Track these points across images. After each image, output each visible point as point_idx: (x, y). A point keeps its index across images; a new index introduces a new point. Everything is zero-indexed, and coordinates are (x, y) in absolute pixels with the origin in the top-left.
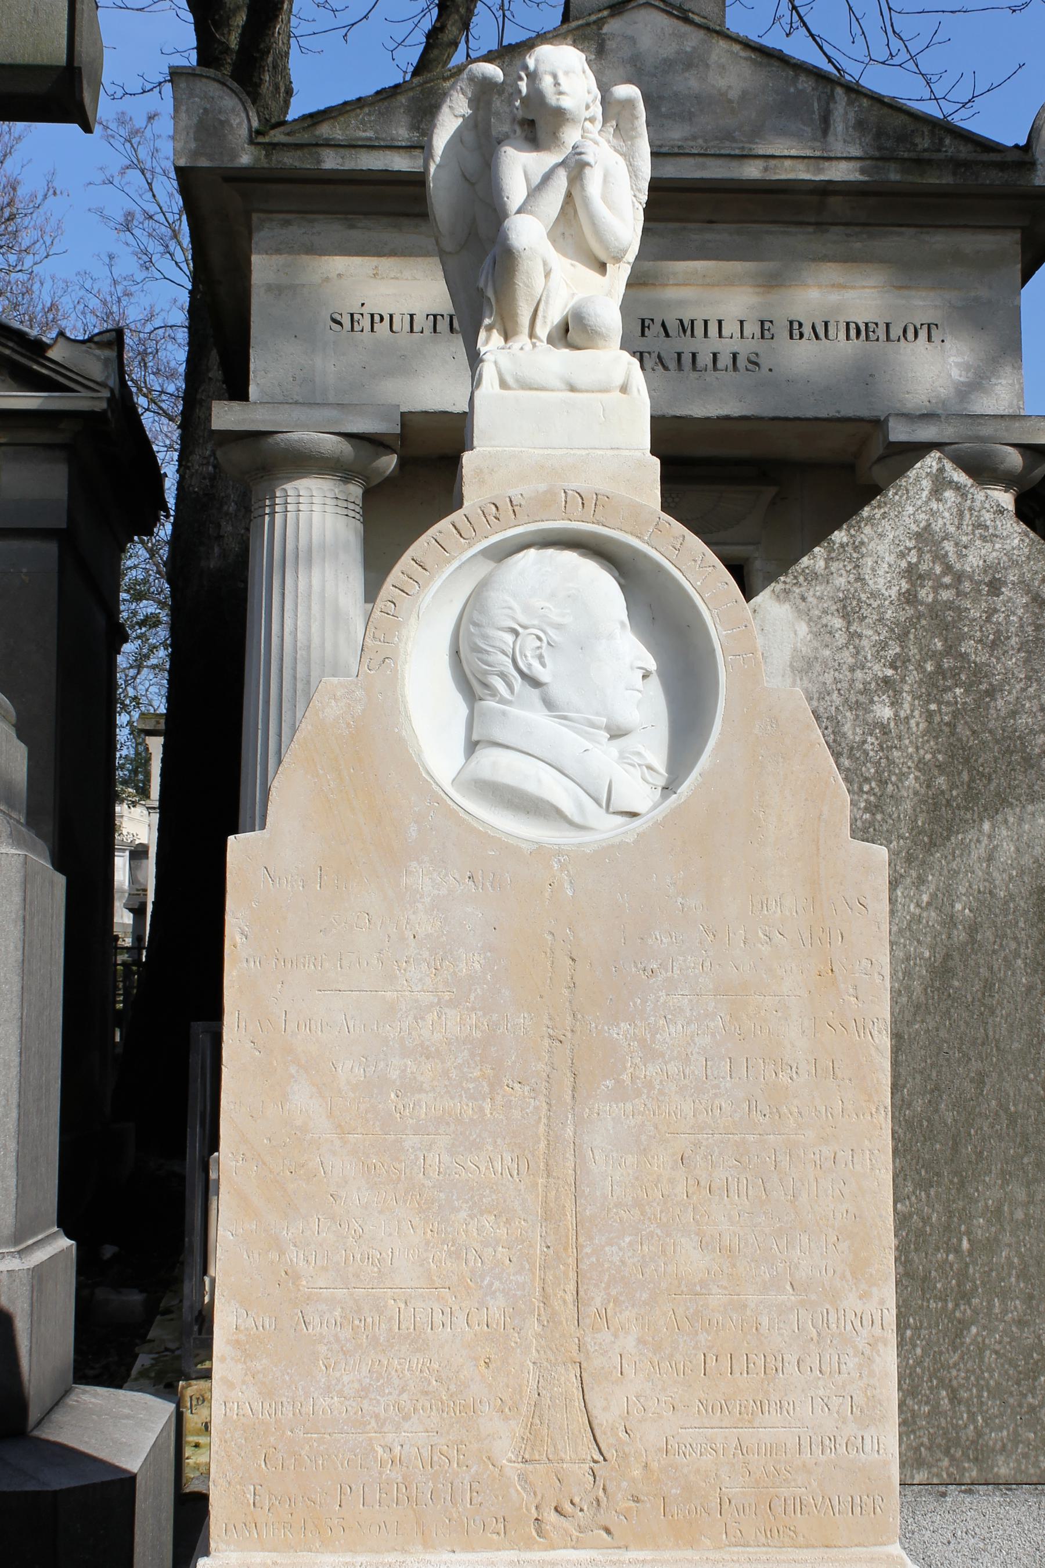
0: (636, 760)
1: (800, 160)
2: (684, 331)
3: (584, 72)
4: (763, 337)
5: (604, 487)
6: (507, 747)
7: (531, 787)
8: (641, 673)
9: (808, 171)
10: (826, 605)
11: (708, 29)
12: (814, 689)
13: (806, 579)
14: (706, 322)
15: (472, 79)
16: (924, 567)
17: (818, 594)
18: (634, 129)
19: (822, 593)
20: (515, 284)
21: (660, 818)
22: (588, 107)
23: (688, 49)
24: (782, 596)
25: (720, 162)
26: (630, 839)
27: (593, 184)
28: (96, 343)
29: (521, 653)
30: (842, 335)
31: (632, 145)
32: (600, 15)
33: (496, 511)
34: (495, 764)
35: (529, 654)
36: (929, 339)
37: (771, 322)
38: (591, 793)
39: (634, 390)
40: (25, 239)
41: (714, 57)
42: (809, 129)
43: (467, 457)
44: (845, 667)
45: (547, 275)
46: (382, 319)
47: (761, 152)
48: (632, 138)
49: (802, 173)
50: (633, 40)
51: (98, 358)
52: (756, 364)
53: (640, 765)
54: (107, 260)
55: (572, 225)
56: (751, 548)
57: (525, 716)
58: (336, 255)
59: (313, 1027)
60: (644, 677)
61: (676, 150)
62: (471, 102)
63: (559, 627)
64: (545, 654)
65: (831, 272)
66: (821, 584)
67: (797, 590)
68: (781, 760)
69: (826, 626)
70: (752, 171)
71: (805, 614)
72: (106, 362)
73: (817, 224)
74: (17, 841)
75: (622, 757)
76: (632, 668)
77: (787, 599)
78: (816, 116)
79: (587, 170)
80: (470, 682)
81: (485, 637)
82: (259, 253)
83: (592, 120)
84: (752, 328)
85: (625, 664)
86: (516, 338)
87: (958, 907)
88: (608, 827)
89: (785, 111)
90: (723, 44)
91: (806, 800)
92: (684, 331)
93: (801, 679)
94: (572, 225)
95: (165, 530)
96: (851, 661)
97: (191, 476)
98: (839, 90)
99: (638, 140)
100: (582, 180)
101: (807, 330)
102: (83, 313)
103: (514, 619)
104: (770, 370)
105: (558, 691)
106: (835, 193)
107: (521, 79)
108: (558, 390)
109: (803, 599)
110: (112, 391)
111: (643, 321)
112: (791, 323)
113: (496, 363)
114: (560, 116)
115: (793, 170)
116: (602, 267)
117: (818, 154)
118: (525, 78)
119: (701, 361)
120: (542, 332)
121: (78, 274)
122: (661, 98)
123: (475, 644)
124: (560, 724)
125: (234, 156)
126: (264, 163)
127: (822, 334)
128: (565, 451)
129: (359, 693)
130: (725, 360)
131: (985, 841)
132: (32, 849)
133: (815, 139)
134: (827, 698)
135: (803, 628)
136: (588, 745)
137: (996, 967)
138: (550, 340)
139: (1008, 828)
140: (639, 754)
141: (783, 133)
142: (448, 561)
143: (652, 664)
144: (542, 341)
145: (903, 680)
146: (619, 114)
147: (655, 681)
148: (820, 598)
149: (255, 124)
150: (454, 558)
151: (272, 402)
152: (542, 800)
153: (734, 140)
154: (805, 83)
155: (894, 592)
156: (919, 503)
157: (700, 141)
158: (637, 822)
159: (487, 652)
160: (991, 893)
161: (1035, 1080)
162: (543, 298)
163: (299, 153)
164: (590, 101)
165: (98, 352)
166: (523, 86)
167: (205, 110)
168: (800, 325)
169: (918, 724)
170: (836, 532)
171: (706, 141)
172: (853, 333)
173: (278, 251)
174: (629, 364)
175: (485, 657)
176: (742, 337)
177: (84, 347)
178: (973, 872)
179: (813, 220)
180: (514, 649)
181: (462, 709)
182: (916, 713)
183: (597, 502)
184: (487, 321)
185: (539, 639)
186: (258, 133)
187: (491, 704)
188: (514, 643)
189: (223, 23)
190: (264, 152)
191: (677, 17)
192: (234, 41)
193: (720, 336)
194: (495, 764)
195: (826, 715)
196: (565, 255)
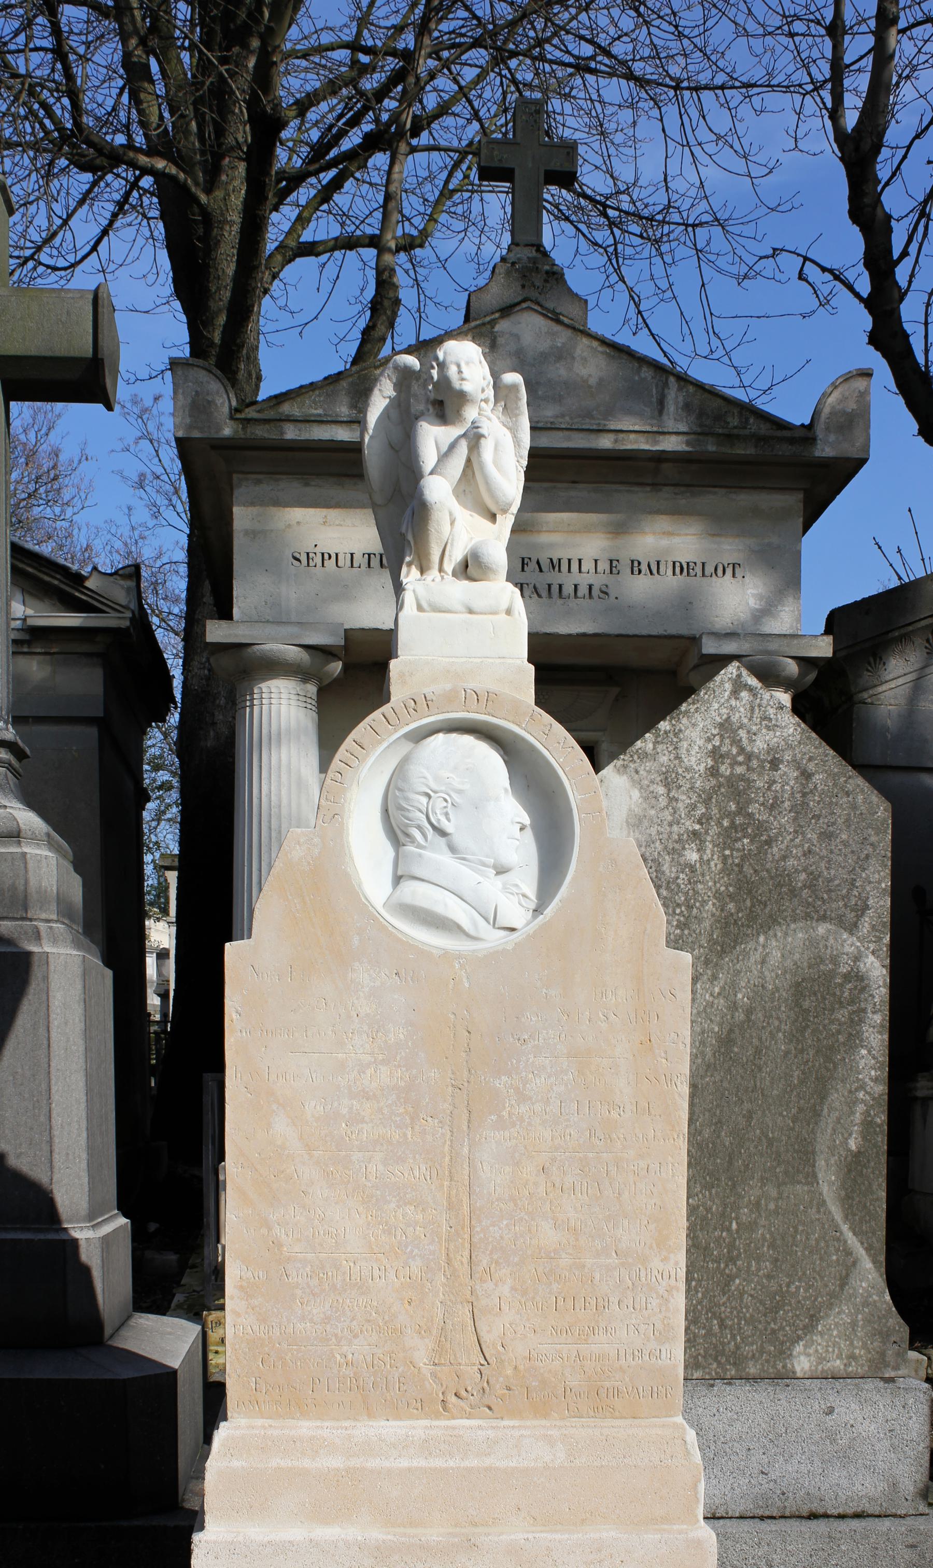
0: (515, 890)
2: (554, 568)
3: (480, 362)
4: (611, 573)
5: (493, 687)
6: (423, 880)
7: (439, 909)
8: (519, 826)
9: (647, 443)
14: (569, 560)
15: (396, 367)
16: (724, 749)
18: (518, 408)
20: (428, 530)
21: (531, 932)
22: (483, 391)
23: (559, 345)
24: (622, 769)
25: (581, 435)
26: (510, 947)
28: (120, 575)
30: (670, 571)
31: (516, 421)
32: (493, 317)
33: (414, 705)
35: (438, 812)
36: (734, 576)
40: (66, 495)
41: (578, 352)
43: (393, 663)
44: (665, 823)
45: (452, 523)
46: (330, 557)
47: (612, 428)
48: (517, 416)
49: (643, 445)
51: (122, 587)
52: (606, 593)
55: (471, 482)
56: (600, 734)
59: (288, 1078)
60: (521, 829)
61: (549, 425)
62: (395, 385)
63: (460, 792)
64: (450, 812)
65: (663, 523)
70: (605, 442)
71: (637, 783)
72: (128, 590)
73: (653, 485)
74: (77, 945)
75: (505, 888)
76: (512, 823)
77: (625, 772)
78: (654, 400)
79: (483, 441)
80: (396, 833)
81: (407, 799)
82: (239, 505)
83: (486, 401)
84: (603, 566)
85: (507, 820)
87: (740, 996)
88: (494, 938)
90: (585, 341)
92: (554, 568)
94: (471, 482)
95: (174, 718)
96: (670, 818)
98: (672, 379)
101: (644, 567)
103: (428, 786)
105: (459, 839)
106: (667, 460)
107: (433, 368)
110: (133, 612)
111: (523, 559)
112: (632, 562)
113: (414, 591)
114: (462, 398)
115: (636, 442)
116: (493, 517)
117: (655, 429)
120: (449, 567)
121: (106, 522)
122: (538, 383)
125: (219, 429)
128: (465, 659)
129: (316, 840)
130: (583, 590)
131: (760, 949)
132: (88, 950)
133: (653, 418)
134: (652, 845)
135: (636, 794)
136: (481, 879)
137: (764, 1038)
139: (777, 940)
140: (517, 886)
141: (629, 412)
143: (527, 820)
145: (707, 833)
146: (506, 396)
147: (529, 833)
148: (649, 772)
151: (248, 622)
152: (447, 919)
154: (647, 373)
155: (702, 768)
156: (722, 701)
157: (567, 418)
158: (515, 935)
159: (408, 810)
160: (763, 986)
161: (787, 1116)
163: (267, 426)
165: (122, 582)
168: (639, 563)
169: (716, 865)
171: (571, 418)
172: (678, 570)
173: (253, 504)
174: (512, 592)
175: (406, 814)
177: (111, 579)
178: (751, 972)
180: (427, 808)
182: (715, 857)
183: (488, 699)
184: (408, 559)
185: (446, 800)
186: (237, 410)
187: (410, 848)
188: (428, 803)
189: (209, 323)
191: (551, 319)
192: (217, 337)
193: (580, 571)
196: (466, 507)
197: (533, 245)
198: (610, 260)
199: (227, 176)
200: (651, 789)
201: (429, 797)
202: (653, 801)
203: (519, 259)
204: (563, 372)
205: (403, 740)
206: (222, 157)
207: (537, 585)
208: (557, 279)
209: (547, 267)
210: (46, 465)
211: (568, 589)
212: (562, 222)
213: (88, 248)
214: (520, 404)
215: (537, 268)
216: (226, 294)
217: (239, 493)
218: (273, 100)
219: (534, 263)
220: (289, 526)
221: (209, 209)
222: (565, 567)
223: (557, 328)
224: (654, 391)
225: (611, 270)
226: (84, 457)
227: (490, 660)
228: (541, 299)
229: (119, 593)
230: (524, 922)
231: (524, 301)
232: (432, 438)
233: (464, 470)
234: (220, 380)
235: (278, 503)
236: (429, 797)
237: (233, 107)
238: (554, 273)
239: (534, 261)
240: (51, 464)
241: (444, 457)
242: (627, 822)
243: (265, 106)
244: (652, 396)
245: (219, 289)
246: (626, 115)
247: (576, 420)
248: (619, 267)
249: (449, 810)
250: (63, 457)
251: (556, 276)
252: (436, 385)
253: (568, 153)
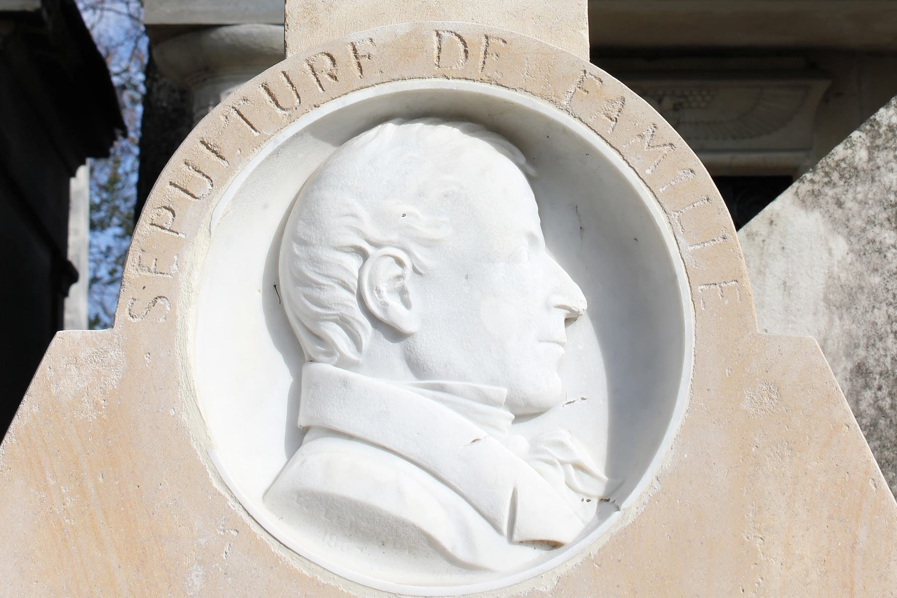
0: (557, 454)
5: (499, 26)
7: (386, 503)
8: (562, 315)
10: (871, 212)
12: (860, 332)
13: (842, 177)
17: (860, 197)
19: (866, 196)
21: (594, 551)
24: (809, 200)
26: (546, 586)
33: (331, 68)
34: (334, 467)
35: (383, 287)
38: (486, 513)
53: (563, 463)
56: (801, 155)
57: (375, 386)
60: (568, 321)
63: (430, 244)
64: (410, 287)
66: (864, 182)
67: (830, 192)
68: (787, 453)
69: (874, 242)
71: (843, 226)
75: (535, 449)
76: (548, 307)
77: (816, 205)
80: (296, 336)
81: (315, 262)
85: (534, 301)
91: (831, 518)
93: (841, 318)
97: (159, 89)
103: (359, 232)
105: (432, 345)
123: (301, 272)
124: (434, 398)
129: (114, 354)
134: (879, 345)
135: (840, 245)
136: (479, 431)
140: (561, 445)
143: (579, 301)
147: (585, 329)
148: (864, 203)
150: (267, 139)
152: (405, 524)
158: (558, 558)
159: (319, 285)
170: (882, 111)
175: (316, 293)
181: (279, 374)
183: (491, 49)
185: (400, 263)
188: (361, 270)
194: (334, 467)
195: (879, 369)
200: (870, 235)
201: (363, 254)
205: (310, 139)
230: (578, 526)
236: (363, 254)
242: (826, 299)
249: (409, 282)
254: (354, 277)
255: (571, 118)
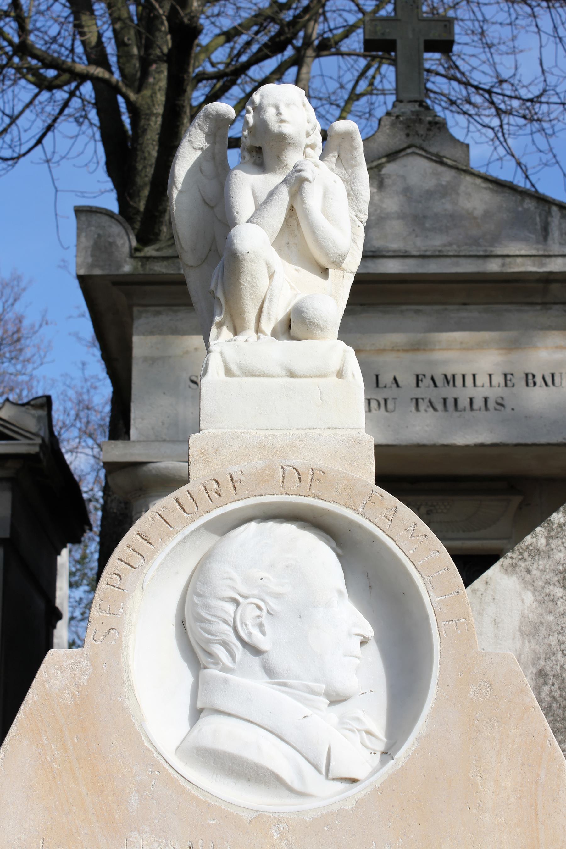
0: (355, 725)
1: (528, 258)
2: (448, 382)
3: (304, 105)
4: (506, 385)
5: (320, 463)
6: (229, 715)
7: (250, 755)
8: (358, 640)
9: (534, 265)
10: (548, 577)
11: (457, 169)
13: (530, 555)
14: (464, 376)
15: (208, 116)
17: (541, 567)
18: (353, 158)
19: (545, 567)
20: (241, 284)
21: (378, 785)
22: (308, 135)
23: (444, 183)
24: (510, 569)
25: (469, 261)
26: (349, 806)
27: (313, 198)
28: (33, 406)
29: (242, 622)
31: (353, 172)
32: (380, 162)
33: (217, 488)
35: (249, 623)
37: (512, 374)
38: (312, 761)
39: (349, 374)
40: (28, 353)
41: (462, 188)
42: (533, 236)
43: (194, 438)
45: (271, 277)
47: (499, 253)
48: (353, 166)
49: (531, 267)
50: (404, 178)
51: (33, 416)
52: (502, 405)
54: (80, 366)
55: (294, 231)
56: (505, 541)
57: (244, 683)
58: (193, 334)
60: (362, 643)
61: (437, 253)
62: (208, 136)
63: (277, 596)
65: (555, 338)
66: (543, 558)
67: (522, 564)
68: (496, 724)
69: (549, 595)
70: (493, 266)
71: (531, 585)
72: (39, 419)
73: (543, 304)
75: (342, 722)
76: (350, 635)
77: (514, 572)
78: (538, 227)
79: (306, 185)
80: (195, 653)
81: (207, 607)
82: (138, 335)
83: (312, 146)
84: (498, 379)
85: (342, 629)
86: (244, 333)
88: (326, 794)
89: (518, 224)
90: (469, 179)
91: (523, 764)
92: (448, 382)
93: (529, 642)
94: (294, 231)
97: (112, 501)
98: (554, 209)
99: (358, 168)
100: (301, 194)
101: (539, 380)
102: (64, 401)
103: (234, 589)
104: (513, 409)
105: (277, 658)
106: (555, 281)
107: (248, 112)
108: (279, 376)
109: (529, 572)
110: (43, 439)
111: (417, 376)
112: (527, 375)
113: (221, 353)
114: (282, 141)
115: (523, 265)
116: (324, 272)
117: (541, 253)
118: (252, 111)
119: (461, 404)
120: (267, 326)
121: (62, 375)
122: (425, 217)
123: (198, 614)
124: (280, 691)
125: (120, 266)
126: (140, 271)
127: (549, 381)
128: (284, 432)
130: (479, 403)
133: (538, 242)
134: (553, 658)
135: (529, 597)
136: (308, 711)
138: (275, 334)
140: (358, 719)
141: (515, 238)
142: (172, 535)
143: (369, 631)
144: (266, 335)
146: (340, 145)
147: (373, 648)
148: (543, 571)
149: (134, 243)
151: (147, 441)
152: (262, 768)
153: (479, 245)
154: (529, 204)
157: (455, 247)
158: (356, 789)
159: (210, 622)
162: (268, 297)
163: (165, 263)
164: (309, 129)
165: (33, 412)
166: (250, 118)
167: (99, 236)
168: (534, 376)
170: (554, 514)
171: (459, 246)
173: (152, 333)
174: (345, 351)
175: (208, 626)
176: (491, 385)
177: (23, 409)
179: (539, 301)
181: (186, 676)
183: (314, 477)
184: (217, 319)
185: (259, 608)
186: (137, 250)
187: (213, 672)
188: (235, 612)
189: (135, 195)
190: (140, 263)
191: (436, 162)
192: (142, 206)
193: (475, 385)
195: (552, 673)
196: (290, 261)
197: (416, 101)
198: (496, 135)
199: (154, 78)
200: (547, 591)
201: (237, 603)
202: (550, 605)
203: (403, 113)
204: (449, 206)
206: (150, 64)
207: (433, 400)
208: (439, 128)
209: (429, 119)
210: (11, 328)
211: (464, 403)
212: (456, 115)
213: (33, 142)
214: (355, 153)
215: (420, 119)
216: (150, 171)
217: (139, 324)
218: (189, 13)
219: (417, 115)
220: (187, 352)
221: (138, 105)
222: (459, 381)
223: (441, 169)
224: (538, 219)
225: (497, 143)
226: (44, 322)
227: (318, 432)
228: (425, 145)
229: (30, 421)
230: (369, 769)
231: (409, 147)
232: (247, 187)
233: (286, 220)
234: (121, 224)
235: (176, 332)
236: (237, 603)
237: (160, 26)
238: (436, 123)
239: (417, 114)
240: (15, 329)
241: (261, 206)
242: (520, 630)
243: (182, 18)
244: (536, 224)
245: (145, 167)
246: (506, 32)
247: (463, 248)
248: (505, 140)
250: (26, 323)
251: (438, 126)
252: (253, 130)
253: (445, 26)
254: (231, 616)
255: (364, 519)
